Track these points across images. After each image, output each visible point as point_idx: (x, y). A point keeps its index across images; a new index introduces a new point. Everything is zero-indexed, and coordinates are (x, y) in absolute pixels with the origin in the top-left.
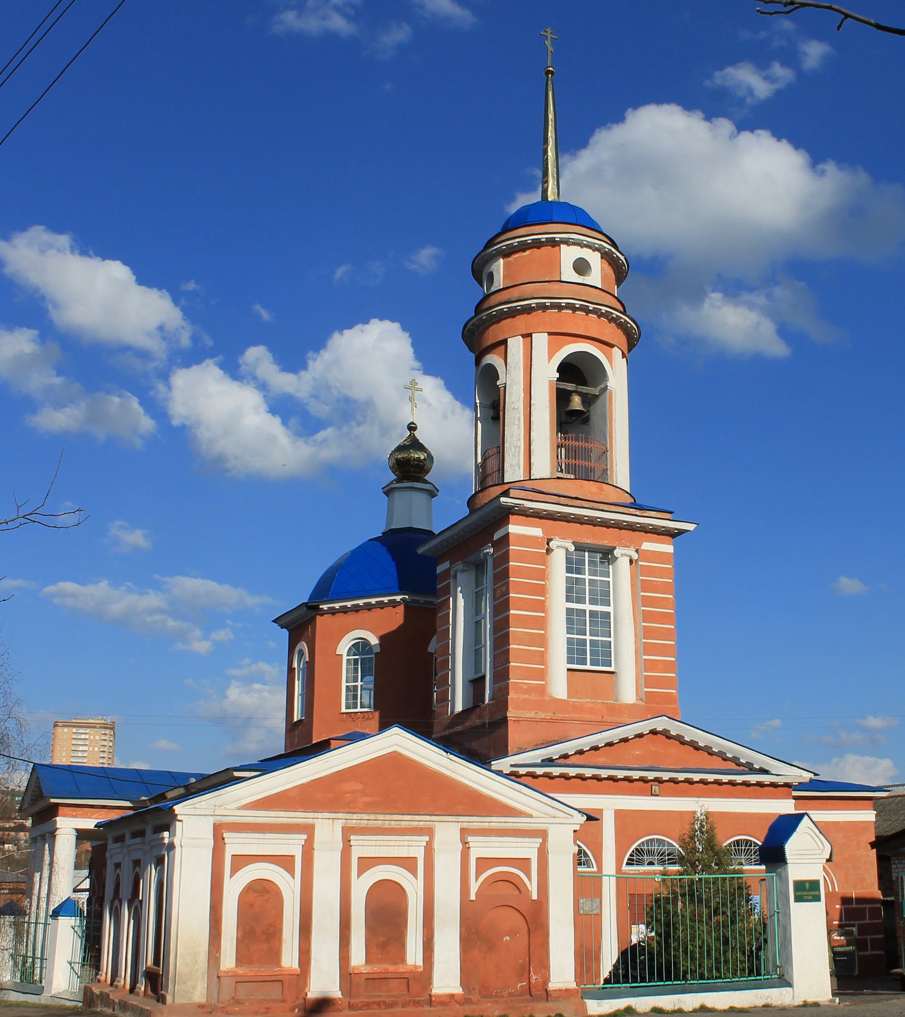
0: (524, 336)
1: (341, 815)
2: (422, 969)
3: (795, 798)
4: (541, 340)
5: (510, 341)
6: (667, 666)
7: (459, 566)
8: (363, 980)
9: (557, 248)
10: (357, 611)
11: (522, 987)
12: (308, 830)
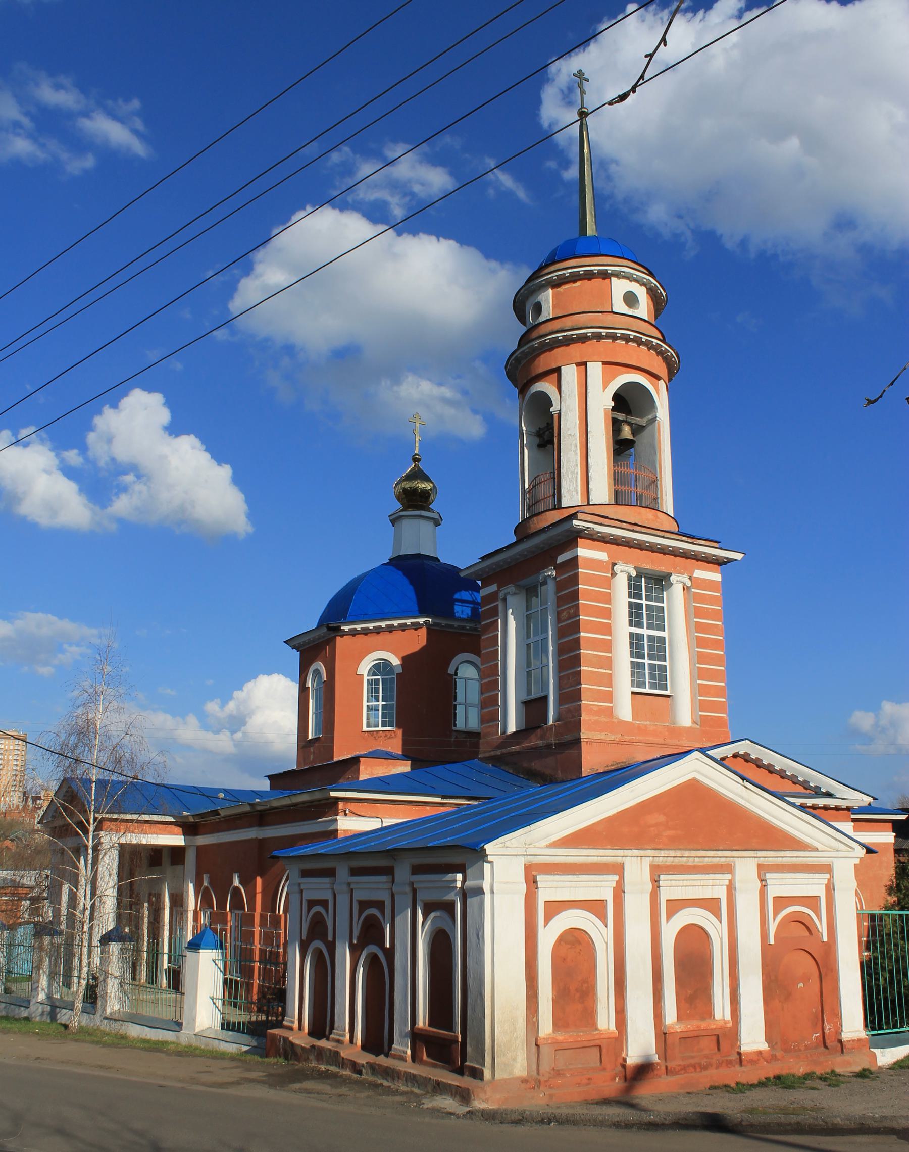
0: (578, 365)
1: (650, 852)
2: (730, 1025)
3: (854, 820)
4: (595, 369)
5: (564, 369)
6: (718, 691)
7: (511, 588)
8: (677, 1040)
9: (607, 281)
10: (378, 633)
11: (816, 1038)
12: (618, 869)
